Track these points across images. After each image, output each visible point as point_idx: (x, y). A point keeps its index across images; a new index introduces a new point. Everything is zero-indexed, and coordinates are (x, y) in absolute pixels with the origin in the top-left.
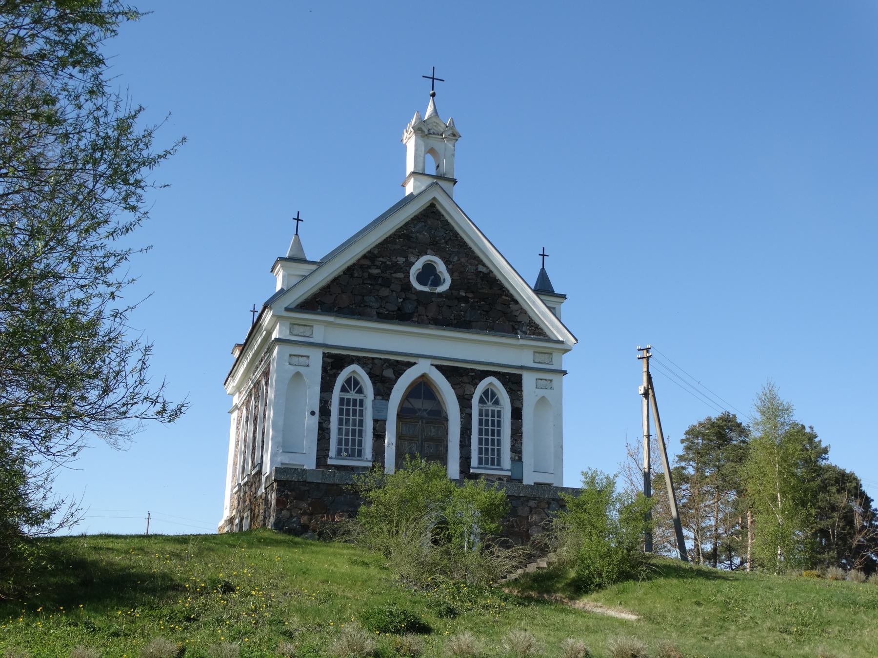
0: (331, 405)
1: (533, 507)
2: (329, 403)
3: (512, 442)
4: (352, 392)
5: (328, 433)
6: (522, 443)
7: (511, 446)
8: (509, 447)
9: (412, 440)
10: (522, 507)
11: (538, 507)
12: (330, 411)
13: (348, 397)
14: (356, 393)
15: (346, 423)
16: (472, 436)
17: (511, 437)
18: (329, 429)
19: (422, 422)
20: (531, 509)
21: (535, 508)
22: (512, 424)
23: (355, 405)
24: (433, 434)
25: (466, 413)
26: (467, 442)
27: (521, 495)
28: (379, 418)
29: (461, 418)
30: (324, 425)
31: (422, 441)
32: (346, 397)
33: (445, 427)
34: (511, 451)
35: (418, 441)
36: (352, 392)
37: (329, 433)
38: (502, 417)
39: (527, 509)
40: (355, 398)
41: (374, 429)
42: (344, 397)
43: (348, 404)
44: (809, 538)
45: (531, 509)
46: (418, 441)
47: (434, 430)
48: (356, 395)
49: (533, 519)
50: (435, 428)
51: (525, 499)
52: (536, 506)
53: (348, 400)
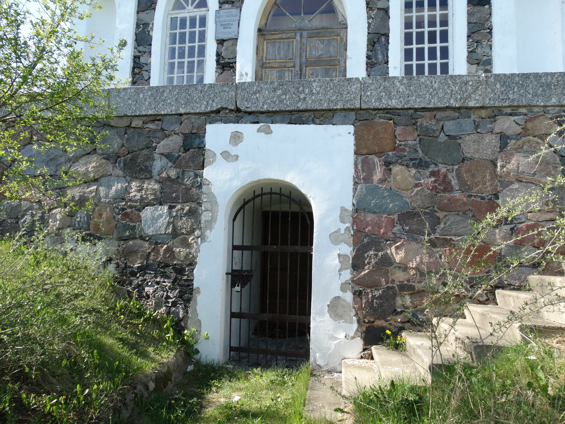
0: (152, 30)
1: (509, 132)
2: (151, 26)
3: (469, 46)
4: (190, 8)
5: (147, 71)
6: (491, 47)
7: (469, 52)
8: (465, 54)
9: (285, 67)
10: (475, 137)
11: (525, 132)
12: (151, 37)
13: (182, 15)
14: (196, 7)
15: (184, 51)
16: (390, 47)
17: (469, 37)
18: (148, 64)
19: (301, 36)
20: (504, 139)
21: (519, 136)
22: (470, 14)
23: (193, 25)
24: (321, 52)
25: (378, 9)
26: (380, 57)
27: (472, 104)
28: (225, 37)
29: (369, 17)
30: (142, 60)
31: (301, 65)
32: (179, 16)
33: (342, 39)
34: (468, 62)
35: (294, 67)
36: (190, 8)
37: (148, 71)
38: (450, 7)
39: (491, 141)
40: (192, 14)
41: (218, 55)
42: (176, 16)
43: (183, 25)
44: (361, 250)
45: (504, 139)
46: (294, 67)
47: (321, 46)
48: (195, 10)
49: (510, 167)
50: (323, 43)
51: (483, 113)
52: (519, 129)
53: (183, 21)
